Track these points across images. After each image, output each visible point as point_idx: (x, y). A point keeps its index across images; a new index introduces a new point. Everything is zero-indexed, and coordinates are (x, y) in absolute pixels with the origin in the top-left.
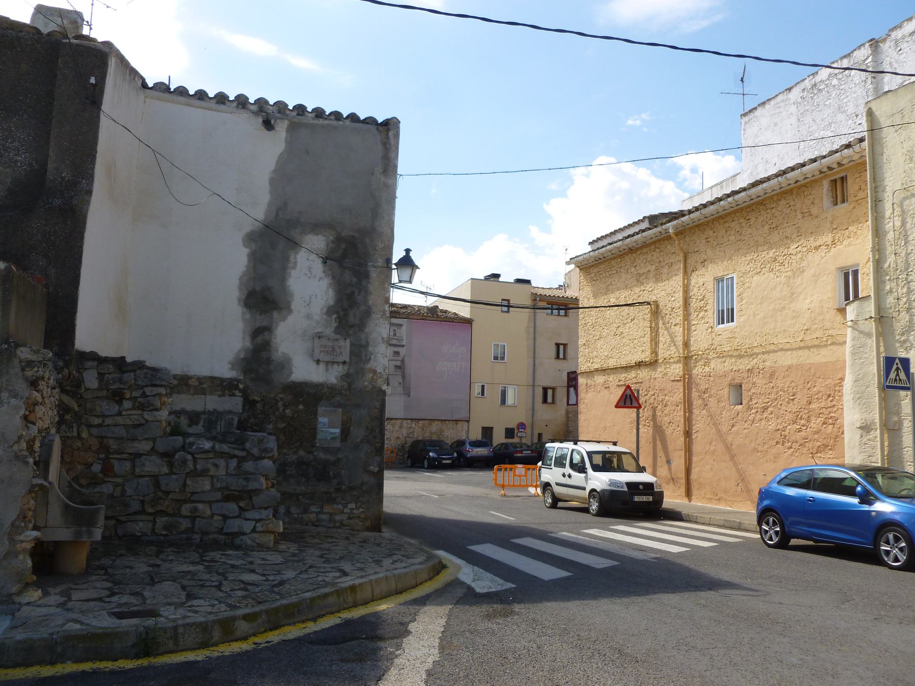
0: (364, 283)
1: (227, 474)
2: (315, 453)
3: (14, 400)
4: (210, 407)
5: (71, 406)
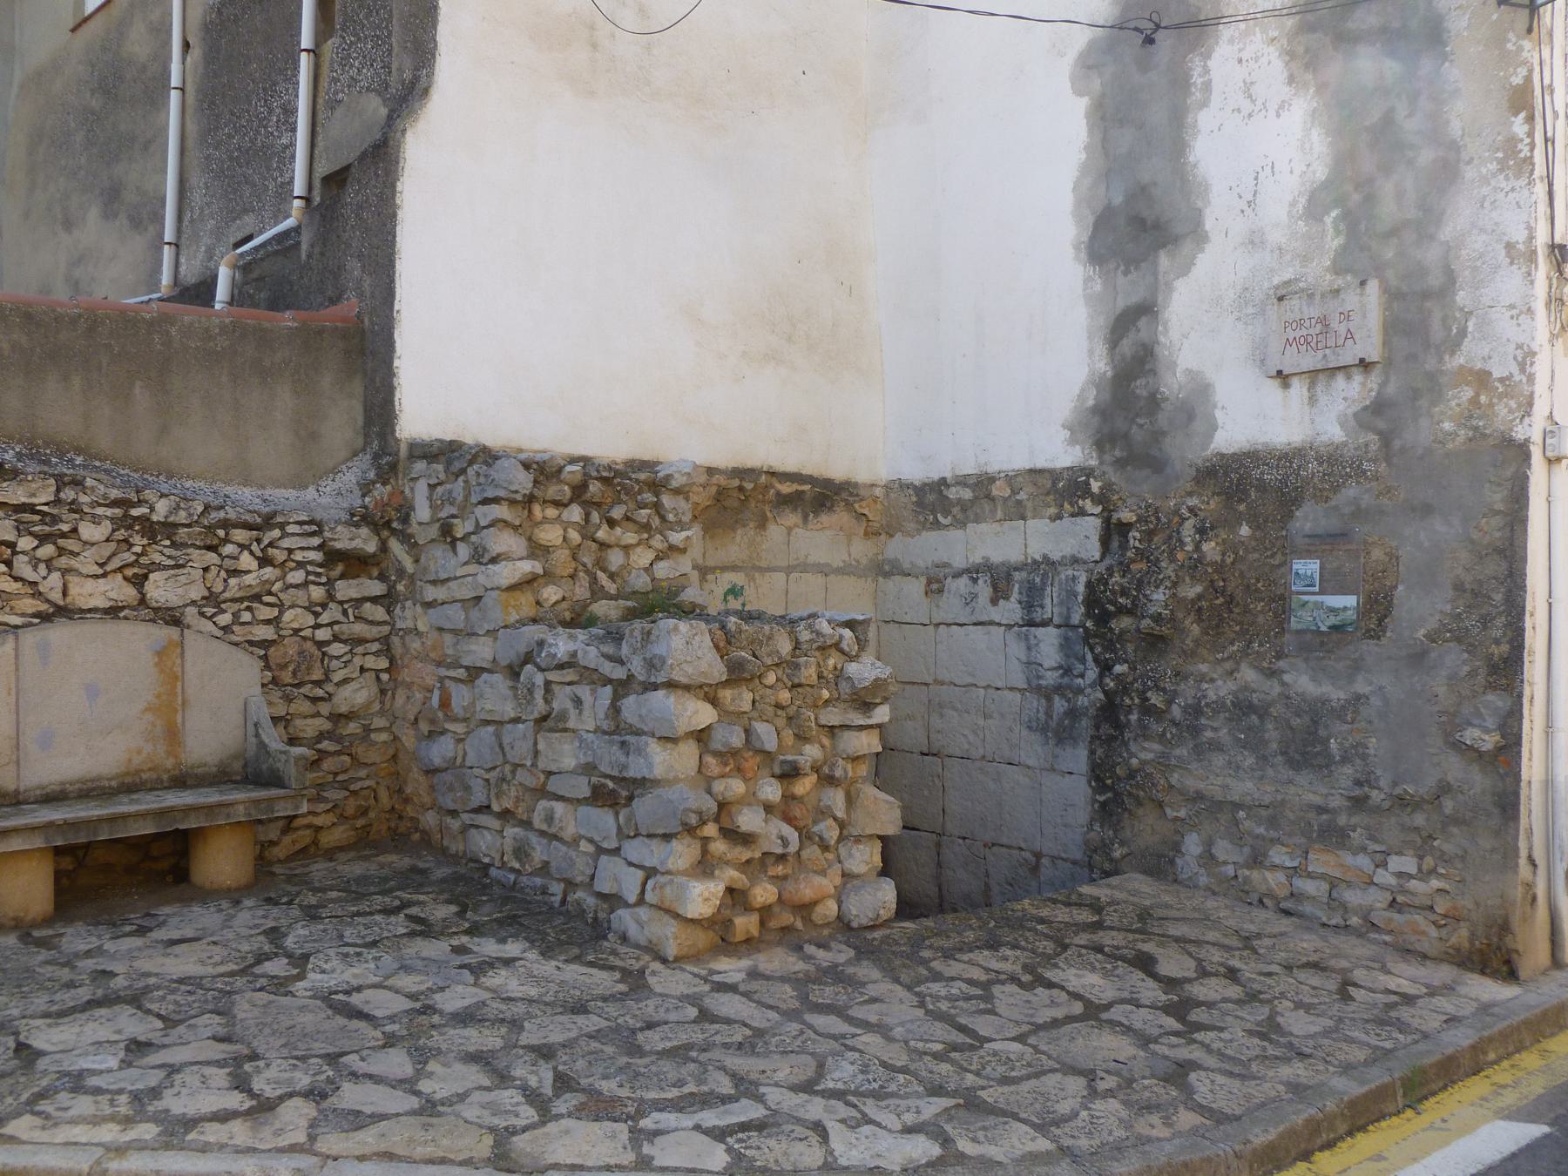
2: (1286, 678)
4: (1035, 552)
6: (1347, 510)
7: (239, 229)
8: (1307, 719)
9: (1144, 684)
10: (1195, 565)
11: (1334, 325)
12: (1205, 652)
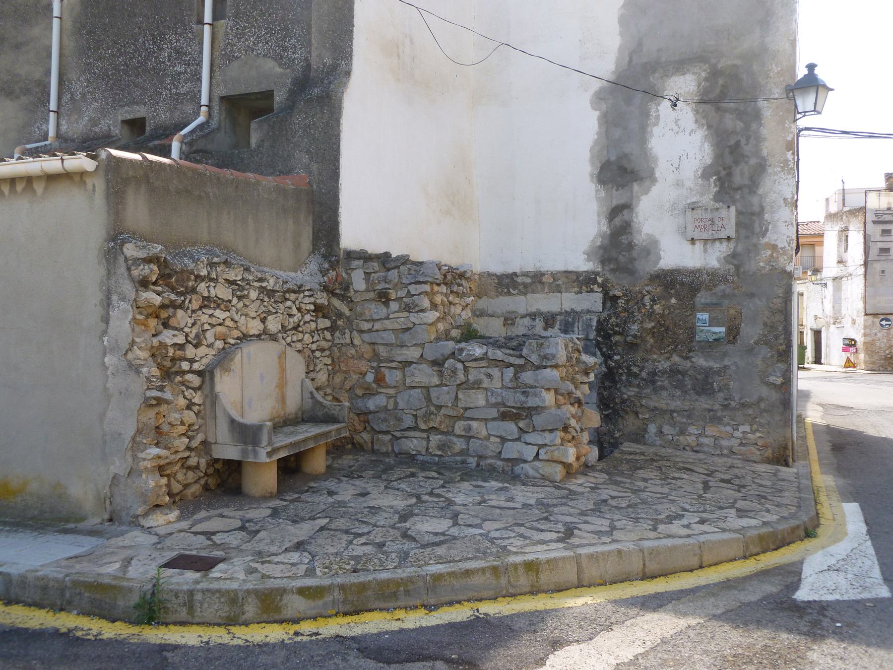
0: (754, 126)
1: (503, 387)
2: (693, 360)
3: (122, 303)
4: (567, 307)
5: (343, 311)
6: (720, 294)
7: (127, 111)
8: (703, 376)
9: (628, 364)
10: (651, 315)
11: (716, 222)
12: (656, 350)
